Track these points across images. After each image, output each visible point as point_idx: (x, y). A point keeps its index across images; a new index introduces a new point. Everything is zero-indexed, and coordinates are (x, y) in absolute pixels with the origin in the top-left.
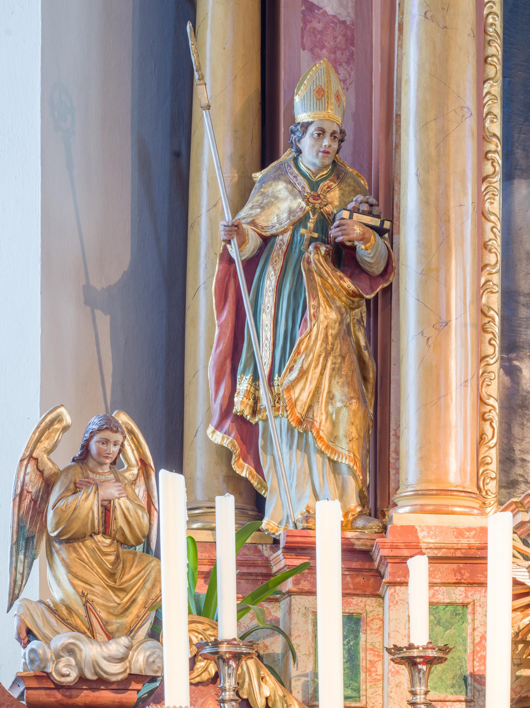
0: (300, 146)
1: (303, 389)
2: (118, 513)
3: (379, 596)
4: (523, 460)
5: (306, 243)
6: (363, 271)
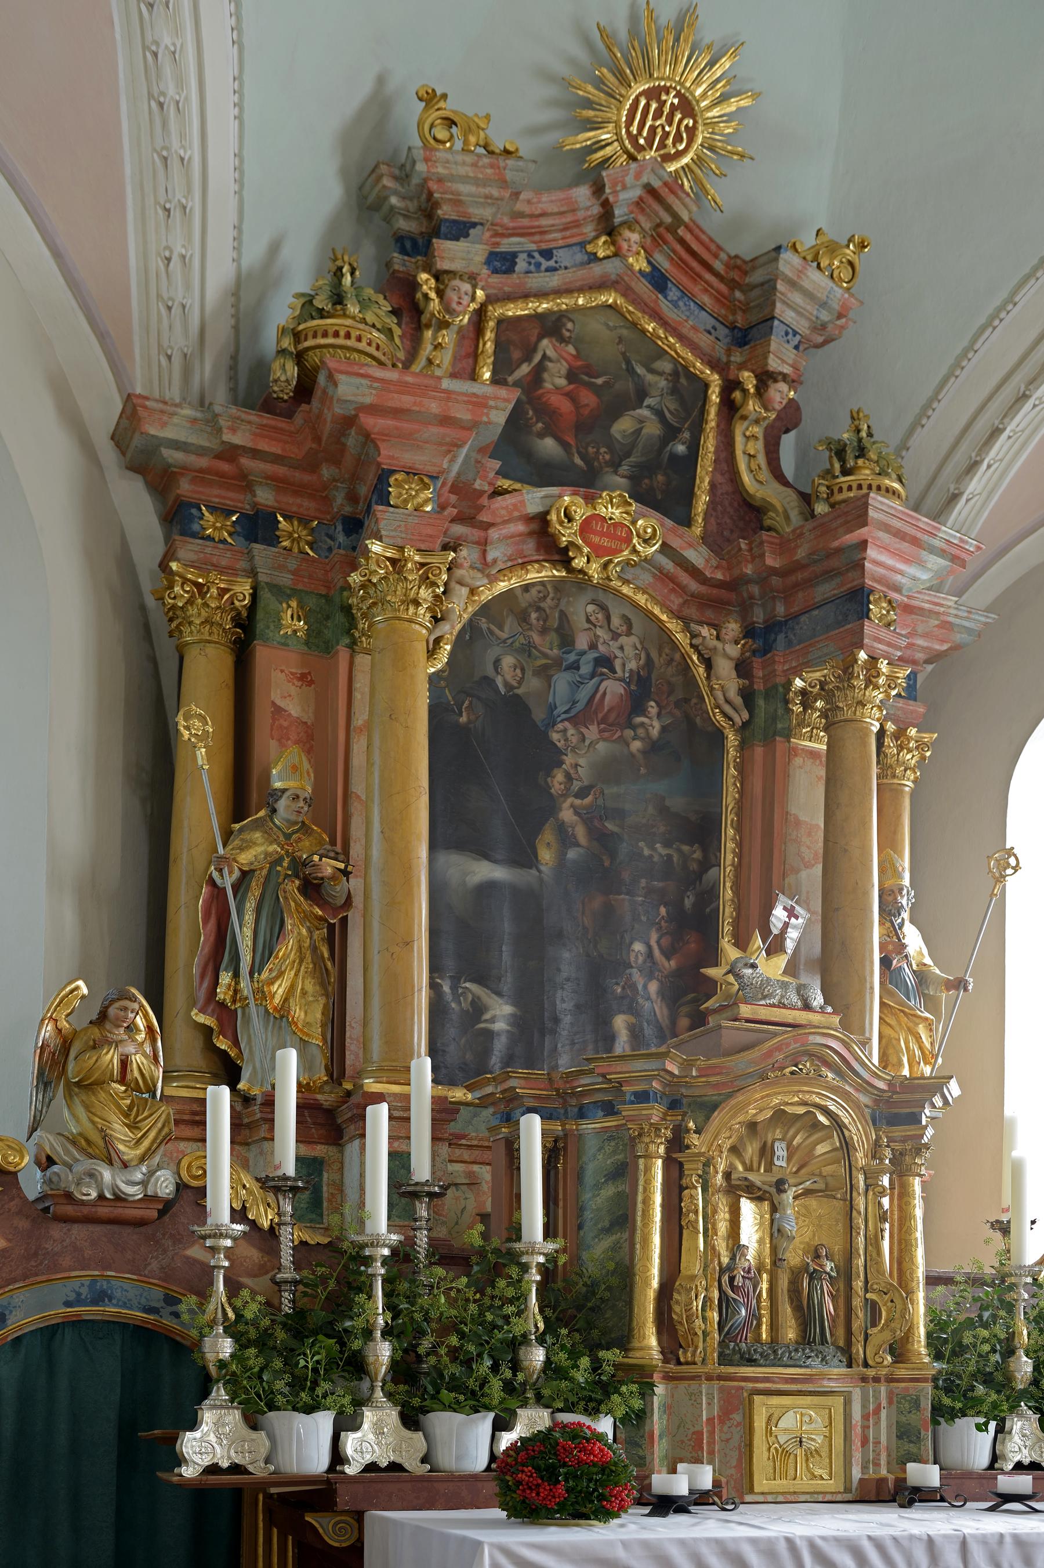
0: (276, 806)
1: (280, 985)
2: (135, 1065)
3: (340, 1145)
4: (444, 1051)
5: (282, 877)
6: (327, 903)
